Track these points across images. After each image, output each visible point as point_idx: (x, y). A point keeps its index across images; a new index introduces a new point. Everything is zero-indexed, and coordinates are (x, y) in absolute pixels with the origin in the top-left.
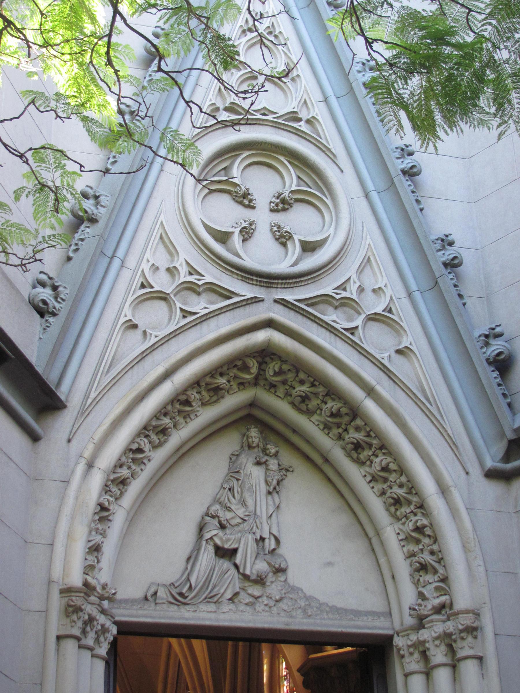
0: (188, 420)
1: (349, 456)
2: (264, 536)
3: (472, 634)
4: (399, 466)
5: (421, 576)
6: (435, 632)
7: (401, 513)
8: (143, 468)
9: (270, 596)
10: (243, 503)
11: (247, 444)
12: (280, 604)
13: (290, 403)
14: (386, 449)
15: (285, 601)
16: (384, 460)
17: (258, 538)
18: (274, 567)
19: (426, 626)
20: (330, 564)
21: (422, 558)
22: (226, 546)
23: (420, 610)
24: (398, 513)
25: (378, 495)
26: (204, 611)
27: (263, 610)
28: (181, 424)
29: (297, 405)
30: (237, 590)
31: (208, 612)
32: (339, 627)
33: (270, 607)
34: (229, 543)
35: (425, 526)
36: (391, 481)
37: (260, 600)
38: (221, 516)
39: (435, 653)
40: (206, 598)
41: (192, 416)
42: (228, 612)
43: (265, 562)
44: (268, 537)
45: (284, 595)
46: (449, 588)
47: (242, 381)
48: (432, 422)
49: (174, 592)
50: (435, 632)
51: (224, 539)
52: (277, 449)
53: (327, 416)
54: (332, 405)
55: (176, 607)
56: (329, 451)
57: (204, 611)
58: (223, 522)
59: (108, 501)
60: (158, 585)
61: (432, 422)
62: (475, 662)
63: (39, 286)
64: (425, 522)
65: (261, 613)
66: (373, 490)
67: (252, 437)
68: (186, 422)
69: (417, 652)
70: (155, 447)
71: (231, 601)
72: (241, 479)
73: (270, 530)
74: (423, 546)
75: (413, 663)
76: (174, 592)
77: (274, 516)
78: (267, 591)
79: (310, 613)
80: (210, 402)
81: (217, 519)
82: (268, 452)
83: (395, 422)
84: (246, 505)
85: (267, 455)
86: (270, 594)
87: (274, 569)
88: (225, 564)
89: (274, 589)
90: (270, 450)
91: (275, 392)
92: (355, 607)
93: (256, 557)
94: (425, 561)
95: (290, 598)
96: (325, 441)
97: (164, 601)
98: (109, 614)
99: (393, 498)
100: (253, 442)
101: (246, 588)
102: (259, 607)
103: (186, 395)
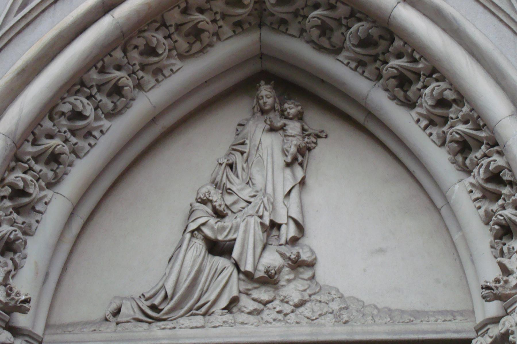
0: (160, 77)
1: (394, 98)
2: (278, 221)
4: (458, 93)
5: (505, 244)
7: (471, 160)
8: (93, 143)
9: (286, 300)
10: (249, 182)
11: (259, 109)
12: (302, 309)
13: (308, 42)
14: (438, 72)
15: (308, 305)
16: (436, 88)
17: (267, 222)
18: (290, 259)
20: (381, 251)
21: (501, 215)
22: (220, 238)
24: (468, 162)
25: (439, 144)
26: (186, 327)
27: (274, 320)
28: (149, 82)
29: (316, 41)
30: (235, 293)
31: (192, 328)
32: (388, 334)
33: (286, 315)
34: (225, 233)
35: (500, 169)
36: (452, 118)
37: (269, 305)
38: (214, 200)
40: (190, 309)
41: (166, 72)
42: (222, 326)
43: (277, 254)
44: (285, 222)
45: (307, 298)
47: (237, 19)
48: (501, 20)
49: (145, 305)
51: (216, 227)
52: (299, 108)
53: (354, 45)
54: (359, 28)
55: (145, 325)
56: (366, 98)
57: (186, 327)
58: (218, 207)
59: (24, 180)
60: (123, 298)
61: (501, 20)
63: (493, 287)
64: (500, 161)
65: (271, 323)
66: (431, 137)
67: (262, 97)
68: (157, 80)
70: (111, 115)
71: (226, 311)
72: (247, 151)
73: (288, 213)
74: (504, 199)
76: (145, 305)
77: (294, 194)
78: (281, 293)
79: (345, 319)
80: (192, 52)
81: (209, 204)
82: (286, 113)
83: (444, 30)
84: (253, 184)
85: (286, 118)
86: (285, 297)
87: (290, 263)
88: (221, 262)
89: (293, 289)
90: (288, 110)
91: (287, 29)
92: (418, 306)
93: (264, 248)
94: (505, 219)
95: (317, 301)
96: (359, 83)
97: (128, 319)
98: (27, 333)
99: (457, 142)
100: (265, 103)
101: (250, 292)
102: (268, 314)
103: (144, 37)
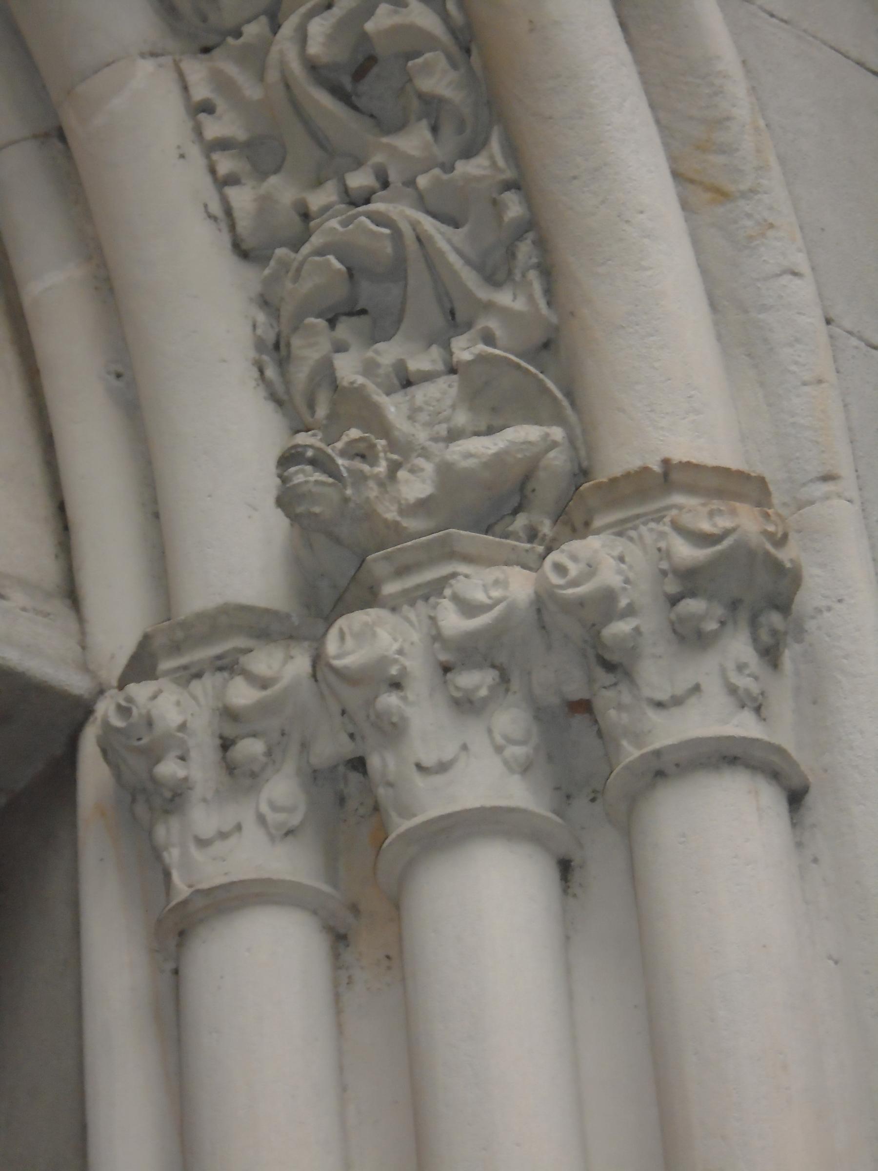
3: (754, 623)
6: (468, 608)
19: (390, 588)
23: (360, 478)
39: (449, 751)
50: (468, 608)
62: (771, 797)
69: (289, 767)
75: (252, 832)
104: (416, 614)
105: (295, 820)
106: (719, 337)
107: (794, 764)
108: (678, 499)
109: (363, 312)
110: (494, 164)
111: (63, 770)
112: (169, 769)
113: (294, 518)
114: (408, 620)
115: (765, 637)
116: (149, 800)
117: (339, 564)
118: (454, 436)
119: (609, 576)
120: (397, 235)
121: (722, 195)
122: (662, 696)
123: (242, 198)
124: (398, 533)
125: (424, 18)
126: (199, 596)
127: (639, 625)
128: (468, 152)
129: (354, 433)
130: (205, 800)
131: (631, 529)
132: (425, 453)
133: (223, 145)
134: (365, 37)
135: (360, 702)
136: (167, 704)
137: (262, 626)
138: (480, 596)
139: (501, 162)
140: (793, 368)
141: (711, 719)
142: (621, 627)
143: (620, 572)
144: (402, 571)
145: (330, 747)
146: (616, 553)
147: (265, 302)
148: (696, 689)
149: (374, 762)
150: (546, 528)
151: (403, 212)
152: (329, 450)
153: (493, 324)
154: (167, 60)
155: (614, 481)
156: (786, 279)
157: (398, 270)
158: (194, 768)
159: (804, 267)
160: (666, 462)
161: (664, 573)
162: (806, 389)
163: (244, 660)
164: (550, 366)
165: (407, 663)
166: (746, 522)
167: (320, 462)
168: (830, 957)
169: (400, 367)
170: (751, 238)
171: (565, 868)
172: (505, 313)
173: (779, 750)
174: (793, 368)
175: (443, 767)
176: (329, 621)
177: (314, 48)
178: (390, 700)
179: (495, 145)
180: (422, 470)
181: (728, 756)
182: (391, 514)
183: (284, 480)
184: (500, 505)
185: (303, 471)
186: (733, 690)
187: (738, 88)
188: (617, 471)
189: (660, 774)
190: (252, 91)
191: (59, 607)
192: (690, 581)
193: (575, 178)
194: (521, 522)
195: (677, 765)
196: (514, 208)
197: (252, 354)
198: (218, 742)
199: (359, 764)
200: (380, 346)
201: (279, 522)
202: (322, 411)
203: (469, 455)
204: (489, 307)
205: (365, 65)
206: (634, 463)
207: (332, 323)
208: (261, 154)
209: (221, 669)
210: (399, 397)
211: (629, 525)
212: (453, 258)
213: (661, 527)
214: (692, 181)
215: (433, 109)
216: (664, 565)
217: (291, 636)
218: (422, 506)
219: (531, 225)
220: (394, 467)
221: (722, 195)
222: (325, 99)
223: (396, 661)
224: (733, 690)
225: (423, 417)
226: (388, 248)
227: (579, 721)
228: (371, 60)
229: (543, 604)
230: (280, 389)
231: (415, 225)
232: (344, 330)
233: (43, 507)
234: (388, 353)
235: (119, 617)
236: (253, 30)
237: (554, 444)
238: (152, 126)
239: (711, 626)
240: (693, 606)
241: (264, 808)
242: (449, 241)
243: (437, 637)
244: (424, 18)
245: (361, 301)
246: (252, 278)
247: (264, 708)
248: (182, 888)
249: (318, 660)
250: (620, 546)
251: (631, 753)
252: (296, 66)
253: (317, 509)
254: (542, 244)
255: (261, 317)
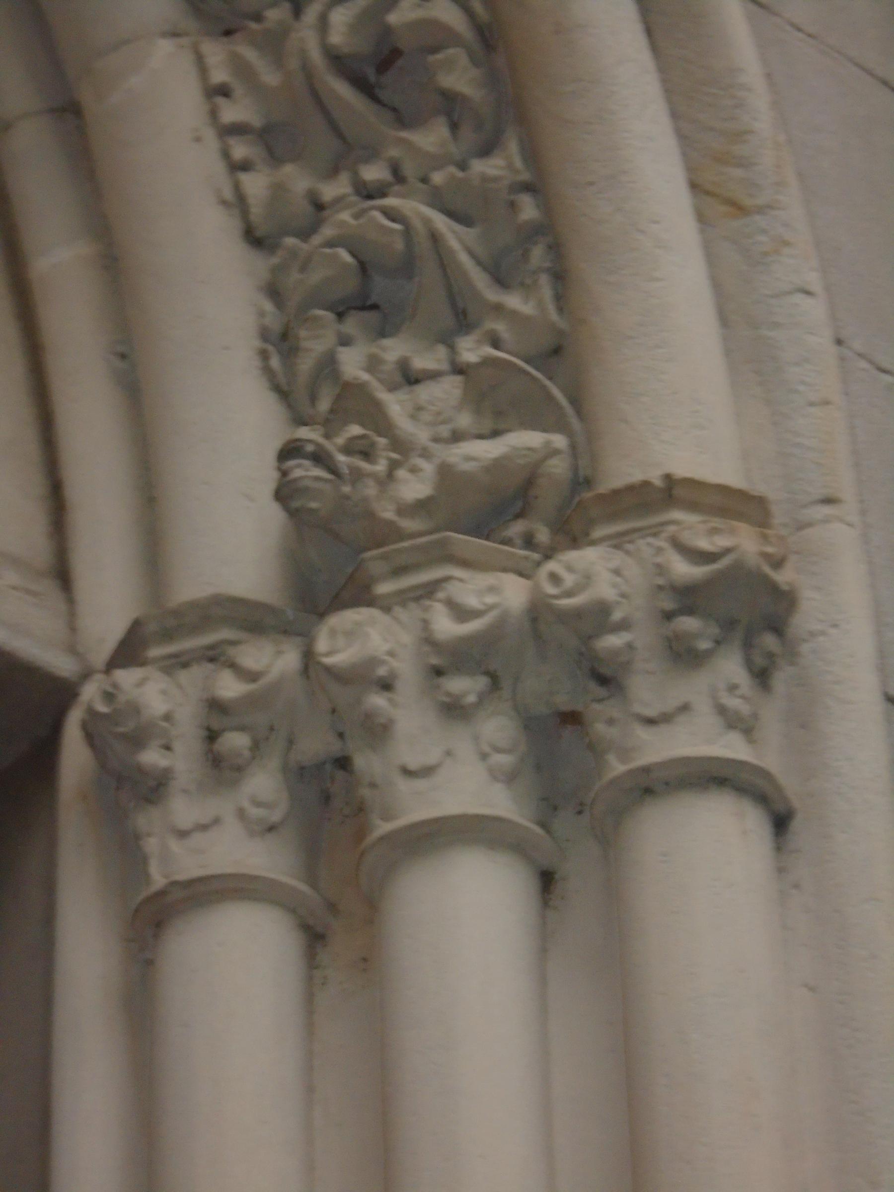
3: (748, 645)
6: (461, 613)
19: (384, 588)
23: (357, 476)
39: (432, 757)
46: (576, 402)
50: (461, 613)
62: (755, 821)
69: (274, 763)
75: (232, 828)
104: (407, 615)
105: (276, 816)
106: (728, 353)
107: (778, 788)
108: (677, 515)
109: (374, 307)
110: (510, 166)
111: (44, 755)
112: (152, 757)
113: (293, 514)
114: (396, 619)
115: (759, 661)
116: (130, 789)
117: (333, 558)
118: (457, 437)
119: (604, 589)
120: (408, 233)
121: (739, 209)
122: (651, 712)
123: (256, 185)
124: (392, 533)
125: (451, 16)
126: (191, 585)
127: (632, 641)
128: (486, 151)
129: (355, 430)
130: (185, 791)
131: (630, 542)
132: (425, 454)
133: (238, 130)
134: (388, 31)
135: (346, 699)
136: (152, 692)
137: (252, 618)
138: (473, 602)
139: (518, 163)
140: (801, 388)
141: (699, 739)
142: (613, 641)
143: (615, 586)
144: (400, 571)
145: (315, 745)
146: (613, 564)
147: (274, 292)
148: (685, 708)
149: (360, 761)
150: (543, 535)
151: (415, 207)
152: (327, 445)
153: (500, 327)
154: (185, 41)
155: (616, 492)
156: (799, 298)
157: (407, 267)
158: (176, 757)
159: (816, 285)
160: (668, 477)
161: (660, 588)
162: (813, 410)
163: (231, 651)
164: (555, 373)
165: (395, 664)
166: (744, 542)
167: (320, 458)
168: (806, 986)
169: (404, 366)
170: (766, 254)
171: (547, 880)
172: (513, 316)
173: (766, 774)
174: (801, 388)
175: (427, 771)
176: (322, 615)
177: (336, 38)
178: (377, 701)
179: (513, 146)
180: (421, 470)
181: (714, 777)
182: (388, 513)
183: (284, 473)
184: (496, 510)
185: (299, 466)
186: (722, 710)
187: (759, 100)
188: (617, 483)
189: (648, 791)
190: (270, 78)
191: (49, 587)
192: (688, 599)
193: (591, 184)
194: (517, 529)
195: (667, 784)
196: (529, 210)
197: (257, 343)
198: (205, 733)
199: (343, 763)
200: (386, 342)
201: (275, 515)
202: (324, 405)
203: (468, 458)
204: (498, 309)
205: (388, 56)
206: (637, 477)
207: (340, 316)
208: (275, 141)
209: (212, 660)
210: (402, 395)
211: (626, 539)
212: (464, 258)
213: (661, 543)
214: (707, 193)
215: (450, 105)
216: (660, 581)
217: (286, 631)
218: (422, 507)
219: (549, 233)
220: (394, 465)
221: (739, 209)
222: (342, 89)
223: (383, 662)
224: (722, 710)
225: (426, 417)
226: (399, 245)
227: (568, 732)
228: (396, 53)
229: (538, 612)
230: (282, 380)
231: (427, 222)
232: (350, 326)
233: (37, 485)
234: (394, 349)
235: (109, 603)
236: (275, 15)
237: (556, 452)
238: (169, 109)
239: (704, 645)
240: (688, 623)
241: (246, 804)
242: (461, 241)
243: (429, 641)
244: (451, 16)
245: (370, 296)
246: (262, 264)
247: (251, 701)
248: (158, 880)
249: (308, 656)
250: (618, 559)
251: (617, 767)
252: (316, 56)
253: (314, 505)
254: (556, 249)
255: (268, 306)
